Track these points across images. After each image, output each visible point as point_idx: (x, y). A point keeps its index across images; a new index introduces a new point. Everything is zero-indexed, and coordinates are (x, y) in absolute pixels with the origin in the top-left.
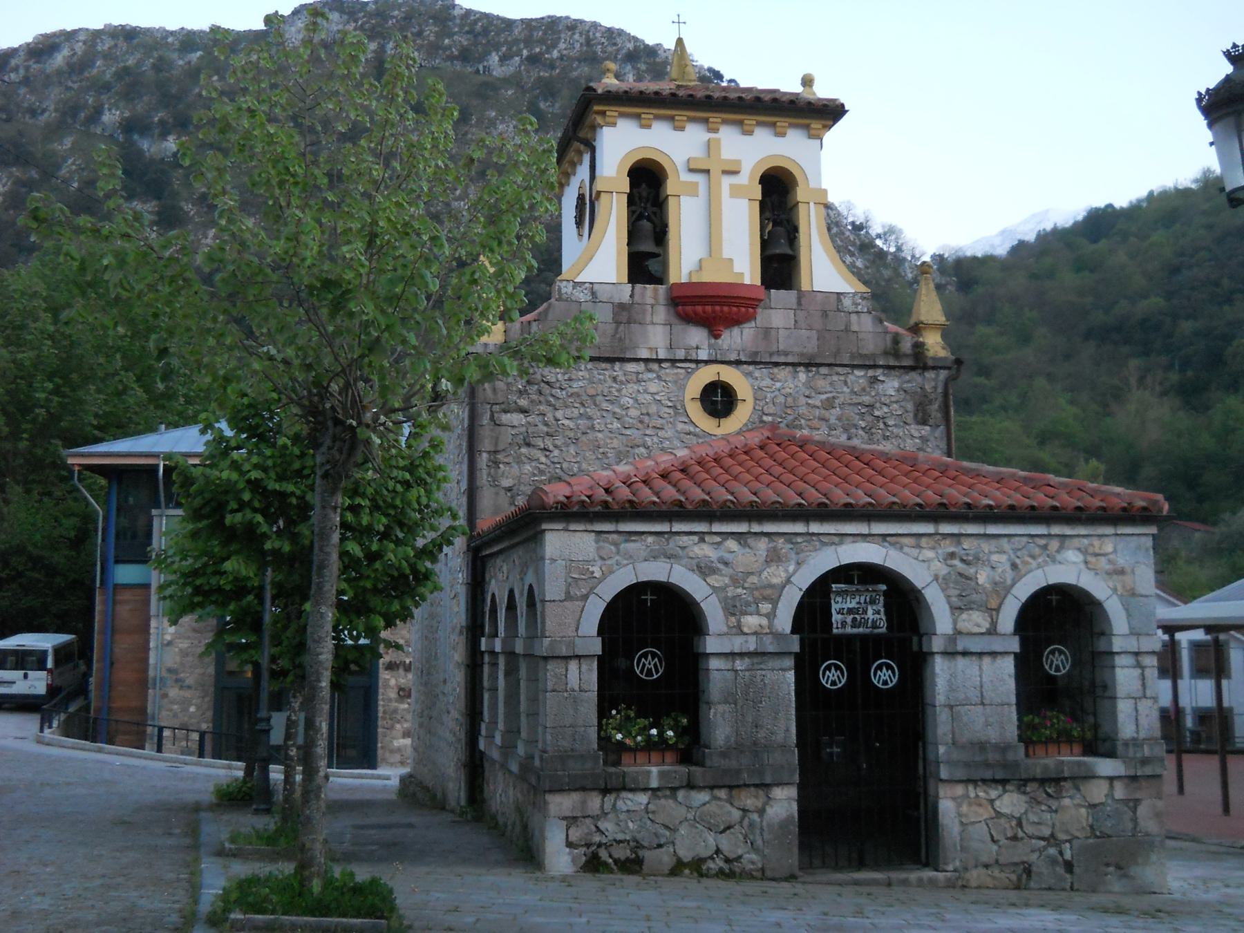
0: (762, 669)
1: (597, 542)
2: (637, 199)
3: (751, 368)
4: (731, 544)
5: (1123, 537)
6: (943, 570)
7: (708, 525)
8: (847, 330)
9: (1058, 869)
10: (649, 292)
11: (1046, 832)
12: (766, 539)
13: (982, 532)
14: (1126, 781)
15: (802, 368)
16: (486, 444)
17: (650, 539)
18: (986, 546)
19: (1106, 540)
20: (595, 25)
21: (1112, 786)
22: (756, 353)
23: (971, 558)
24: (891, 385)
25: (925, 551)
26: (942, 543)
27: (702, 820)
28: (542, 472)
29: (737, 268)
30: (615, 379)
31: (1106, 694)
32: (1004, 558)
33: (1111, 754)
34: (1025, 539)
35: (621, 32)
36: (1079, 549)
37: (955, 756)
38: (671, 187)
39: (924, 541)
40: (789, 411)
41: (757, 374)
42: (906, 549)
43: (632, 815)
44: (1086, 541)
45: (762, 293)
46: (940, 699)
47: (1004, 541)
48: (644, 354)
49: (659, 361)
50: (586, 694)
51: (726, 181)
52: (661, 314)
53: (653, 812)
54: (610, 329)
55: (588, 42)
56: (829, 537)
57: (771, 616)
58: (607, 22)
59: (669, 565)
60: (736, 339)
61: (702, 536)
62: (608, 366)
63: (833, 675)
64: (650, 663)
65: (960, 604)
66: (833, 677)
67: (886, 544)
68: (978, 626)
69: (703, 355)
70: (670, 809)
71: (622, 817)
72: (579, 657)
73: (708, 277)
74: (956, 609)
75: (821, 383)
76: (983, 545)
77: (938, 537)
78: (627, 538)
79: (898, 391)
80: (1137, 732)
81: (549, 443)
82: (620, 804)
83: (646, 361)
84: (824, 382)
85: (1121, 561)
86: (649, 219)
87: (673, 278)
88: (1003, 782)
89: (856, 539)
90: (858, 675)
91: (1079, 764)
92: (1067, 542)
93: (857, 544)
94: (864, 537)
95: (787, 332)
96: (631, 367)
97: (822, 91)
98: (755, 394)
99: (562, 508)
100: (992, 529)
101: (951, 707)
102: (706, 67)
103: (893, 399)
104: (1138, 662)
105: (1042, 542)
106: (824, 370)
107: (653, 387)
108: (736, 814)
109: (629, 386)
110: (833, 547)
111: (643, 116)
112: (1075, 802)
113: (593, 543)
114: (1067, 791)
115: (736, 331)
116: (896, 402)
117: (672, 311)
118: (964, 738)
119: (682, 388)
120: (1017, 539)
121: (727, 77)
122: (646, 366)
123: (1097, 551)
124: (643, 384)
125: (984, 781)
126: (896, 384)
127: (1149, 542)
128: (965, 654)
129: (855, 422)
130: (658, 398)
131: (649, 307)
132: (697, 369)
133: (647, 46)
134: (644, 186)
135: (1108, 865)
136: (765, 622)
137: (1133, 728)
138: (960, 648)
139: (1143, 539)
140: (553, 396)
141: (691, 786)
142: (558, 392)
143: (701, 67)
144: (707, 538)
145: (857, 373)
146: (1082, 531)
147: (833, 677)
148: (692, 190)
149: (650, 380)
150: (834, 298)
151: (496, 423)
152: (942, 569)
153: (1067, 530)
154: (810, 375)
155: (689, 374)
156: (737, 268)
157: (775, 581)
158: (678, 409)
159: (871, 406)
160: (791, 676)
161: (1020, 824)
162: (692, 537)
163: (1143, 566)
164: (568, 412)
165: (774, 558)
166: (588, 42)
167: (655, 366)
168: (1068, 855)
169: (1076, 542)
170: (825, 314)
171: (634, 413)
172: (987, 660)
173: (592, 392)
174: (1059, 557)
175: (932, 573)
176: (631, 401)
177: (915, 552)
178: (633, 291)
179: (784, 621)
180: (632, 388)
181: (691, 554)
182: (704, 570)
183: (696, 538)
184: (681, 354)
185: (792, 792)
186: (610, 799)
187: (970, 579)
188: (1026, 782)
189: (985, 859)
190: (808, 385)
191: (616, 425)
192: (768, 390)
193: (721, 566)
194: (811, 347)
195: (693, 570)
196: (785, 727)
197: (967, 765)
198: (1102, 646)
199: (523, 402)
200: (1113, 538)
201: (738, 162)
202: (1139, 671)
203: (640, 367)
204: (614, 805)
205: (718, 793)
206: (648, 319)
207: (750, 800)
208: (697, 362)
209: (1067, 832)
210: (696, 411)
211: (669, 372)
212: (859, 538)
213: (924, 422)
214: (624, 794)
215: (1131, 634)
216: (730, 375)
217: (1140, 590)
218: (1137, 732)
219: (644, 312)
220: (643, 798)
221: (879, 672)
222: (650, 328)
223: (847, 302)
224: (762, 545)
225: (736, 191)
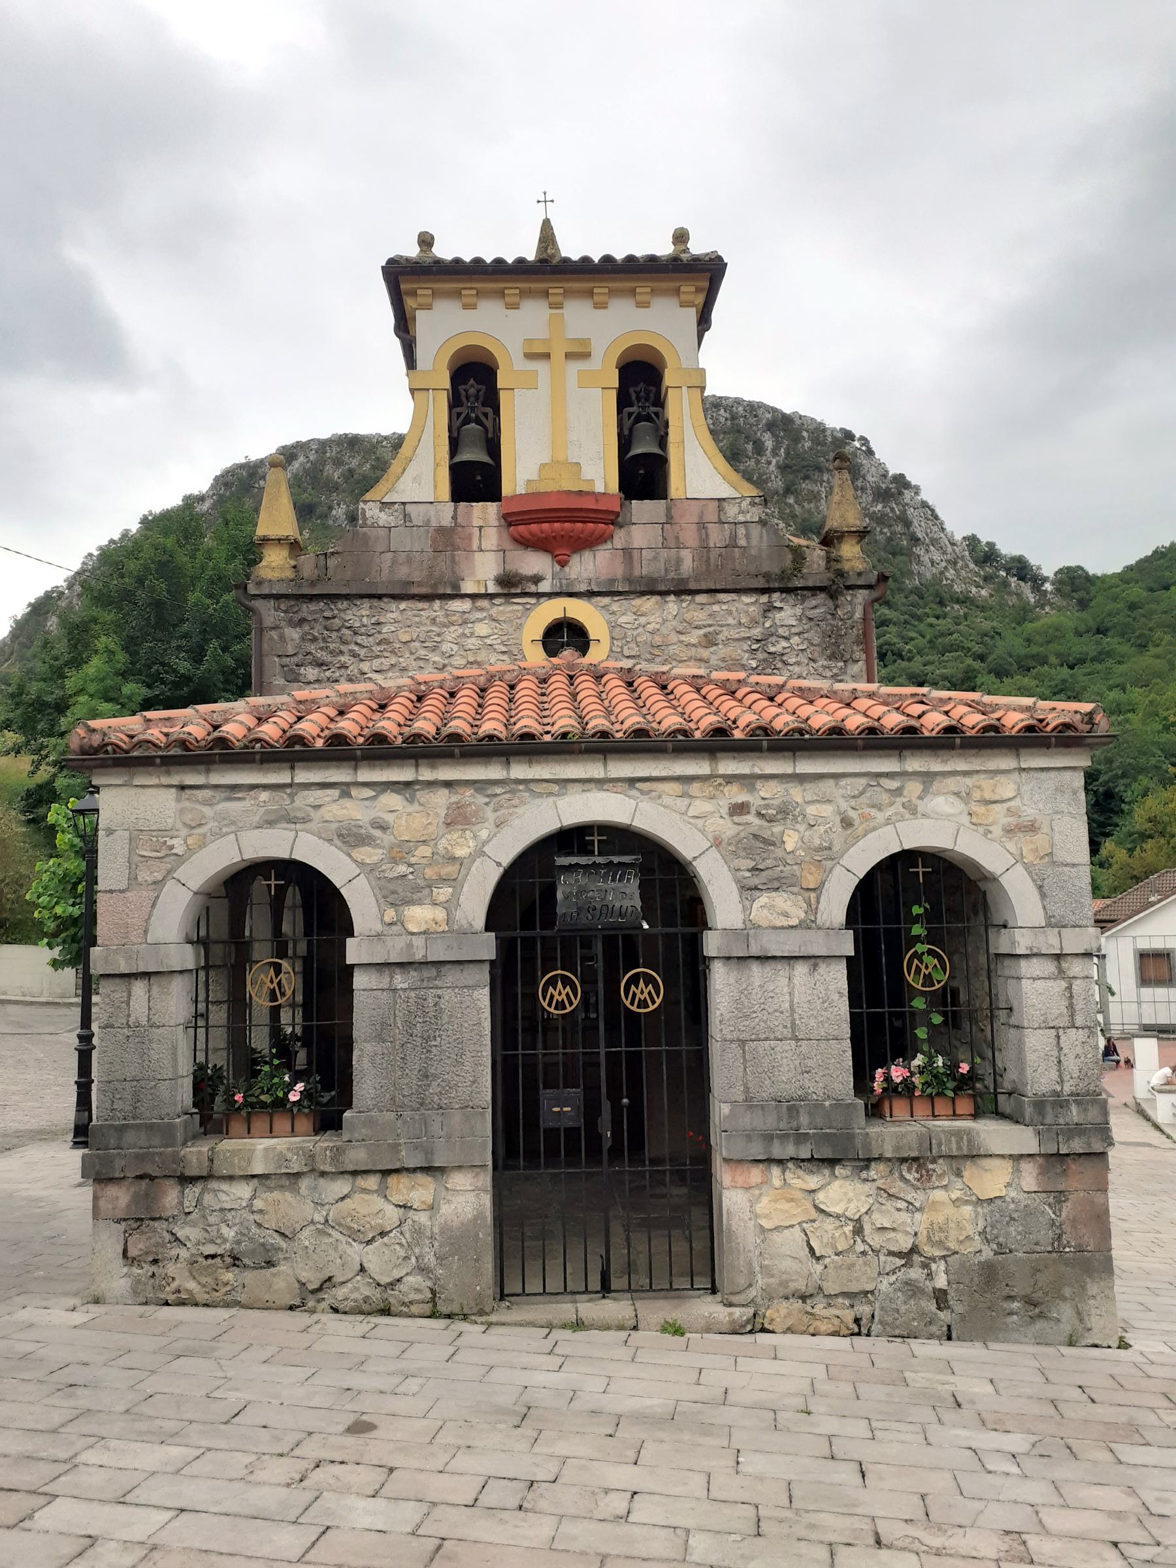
0: (437, 988)
1: (178, 800)
2: (464, 399)
3: (606, 600)
4: (392, 800)
5: (1032, 773)
6: (727, 828)
7: (351, 771)
9: (923, 1303)
10: (485, 513)
11: (905, 1244)
12: (446, 791)
13: (789, 770)
14: (1040, 1160)
15: (672, 598)
17: (264, 796)
18: (797, 793)
19: (1002, 779)
20: (738, 401)
21: (1017, 1171)
22: (613, 581)
23: (772, 812)
24: (788, 613)
25: (697, 802)
26: (726, 789)
27: (340, 1225)
30: (434, 621)
31: (1013, 1021)
32: (827, 810)
33: (1014, 1118)
34: (863, 781)
35: (761, 405)
36: (957, 794)
37: (747, 1120)
39: (695, 788)
40: (656, 652)
41: (615, 607)
42: (666, 800)
43: (229, 1216)
44: (969, 781)
47: (827, 786)
49: (491, 596)
50: (162, 1030)
51: (575, 367)
52: (492, 538)
53: (261, 1211)
55: (734, 417)
56: (545, 785)
57: (449, 906)
58: (748, 397)
59: (293, 834)
61: (345, 789)
62: (425, 605)
63: (560, 993)
65: (756, 881)
67: (634, 792)
68: (786, 915)
69: (545, 587)
71: (212, 1219)
72: (147, 975)
74: (748, 890)
75: (699, 616)
76: (792, 791)
77: (720, 780)
78: (227, 794)
79: (800, 620)
80: (1061, 1082)
82: (208, 1198)
84: (696, 610)
85: (1030, 812)
86: (478, 422)
87: (506, 490)
88: (832, 1162)
89: (587, 786)
91: (958, 1134)
92: (936, 785)
93: (589, 794)
94: (600, 783)
95: (652, 553)
96: (457, 605)
97: (697, 247)
98: (611, 632)
99: (115, 752)
100: (806, 766)
101: (743, 1042)
102: (838, 428)
103: (794, 630)
104: (1061, 971)
105: (894, 784)
107: (482, 629)
108: (392, 1215)
109: (452, 628)
110: (551, 799)
111: (464, 292)
112: (954, 1197)
113: (173, 804)
114: (941, 1176)
115: (587, 555)
116: (798, 634)
117: (505, 534)
118: (766, 1091)
119: (519, 627)
120: (849, 780)
121: (857, 436)
122: (473, 603)
123: (988, 796)
124: (470, 625)
125: (798, 1161)
126: (798, 611)
127: (1079, 780)
128: (764, 959)
129: (744, 662)
130: (488, 641)
131: (476, 531)
132: (538, 604)
133: (784, 415)
134: (472, 381)
135: (1010, 1298)
136: (440, 914)
137: (1054, 1075)
138: (755, 951)
139: (1067, 775)
140: (356, 644)
143: (834, 430)
144: (354, 792)
145: (747, 599)
146: (961, 765)
149: (481, 620)
152: (727, 828)
153: (936, 766)
154: (684, 605)
157: (460, 852)
160: (483, 997)
161: (858, 1231)
162: (329, 791)
163: (1067, 819)
164: (376, 664)
165: (457, 819)
166: (734, 417)
167: (485, 603)
168: (941, 1282)
169: (951, 783)
170: (702, 526)
172: (801, 969)
174: (922, 806)
175: (710, 836)
176: (455, 647)
177: (682, 803)
178: (455, 510)
180: (457, 630)
181: (328, 817)
183: (335, 793)
186: (193, 1192)
187: (774, 844)
188: (867, 1162)
189: (800, 1285)
192: (629, 626)
193: (377, 833)
195: (330, 841)
197: (768, 1138)
198: (1002, 943)
200: (1015, 776)
201: (586, 342)
202: (1064, 984)
203: (466, 605)
204: (199, 1202)
205: (361, 1182)
206: (475, 547)
207: (420, 1191)
209: (940, 1244)
211: (500, 609)
212: (593, 785)
214: (214, 1185)
215: (1049, 925)
216: (579, 610)
217: (1061, 855)
218: (1061, 1082)
219: (470, 538)
220: (243, 1191)
221: (551, 989)
222: (478, 555)
224: (441, 798)
225: (586, 381)
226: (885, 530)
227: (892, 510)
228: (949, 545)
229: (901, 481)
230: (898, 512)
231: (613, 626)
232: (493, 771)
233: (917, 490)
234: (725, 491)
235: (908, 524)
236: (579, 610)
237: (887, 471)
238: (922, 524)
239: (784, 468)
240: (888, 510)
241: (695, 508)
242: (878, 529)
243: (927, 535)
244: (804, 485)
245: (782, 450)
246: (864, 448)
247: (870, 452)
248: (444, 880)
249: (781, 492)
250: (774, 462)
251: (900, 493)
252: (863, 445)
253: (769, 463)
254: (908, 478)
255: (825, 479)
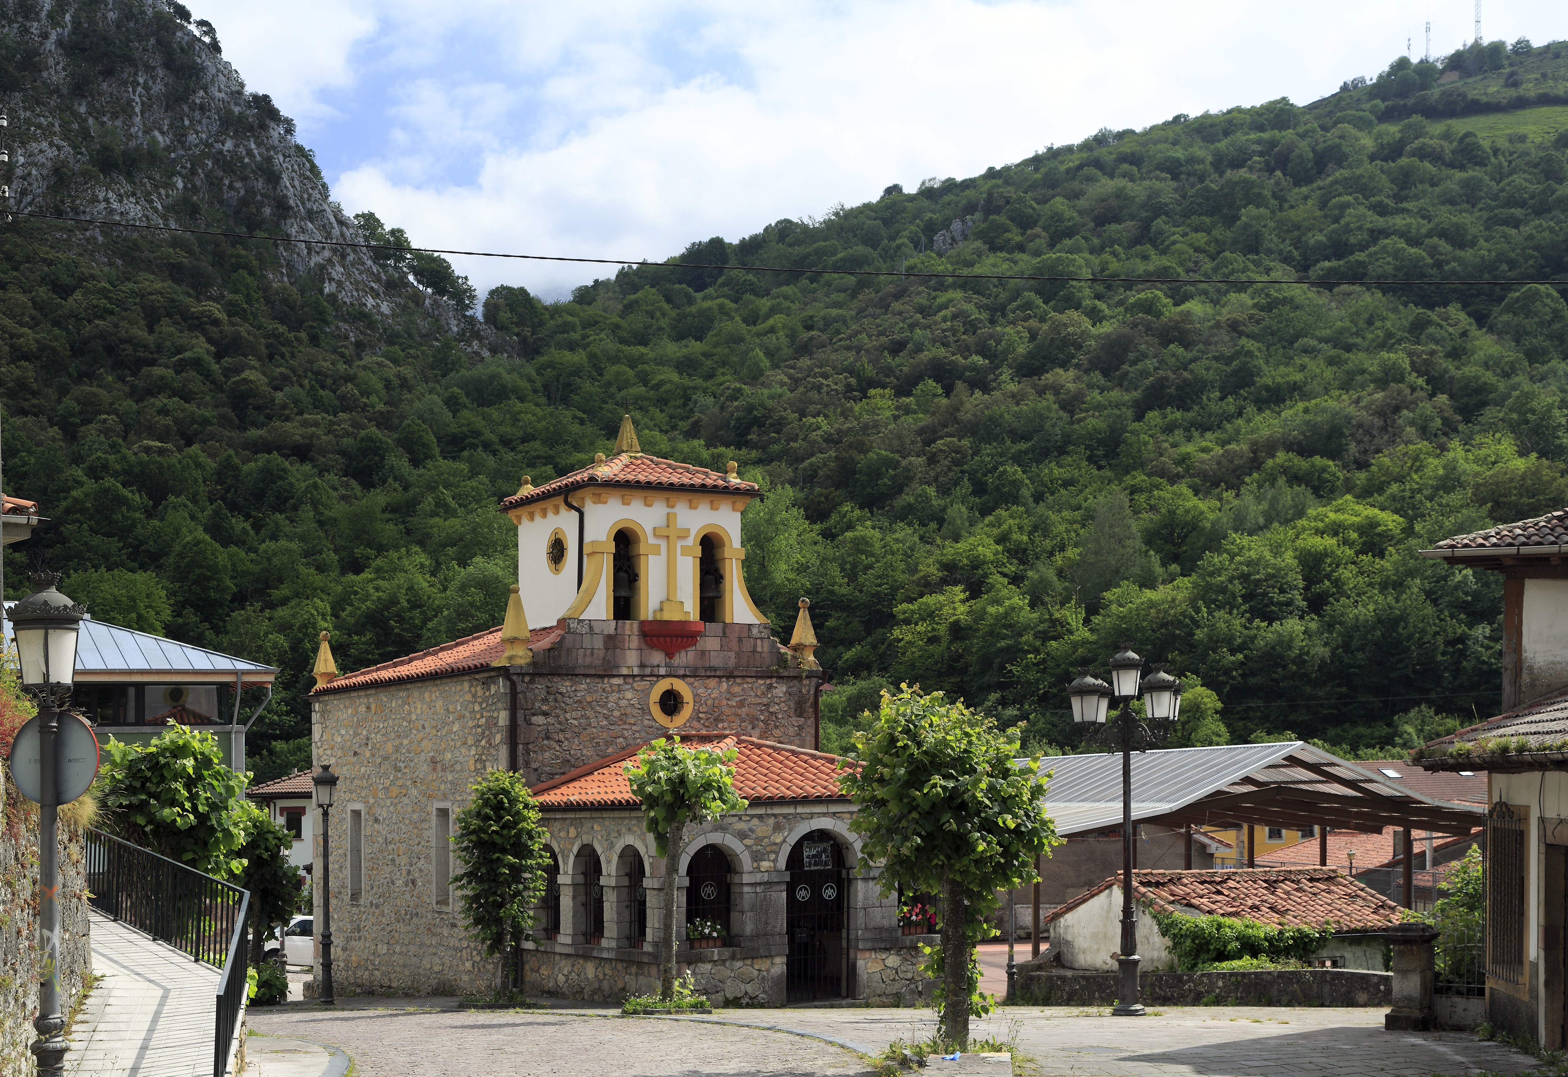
4: (755, 821)
8: (754, 651)
11: (910, 976)
16: (521, 739)
24: (780, 690)
28: (557, 757)
29: (687, 608)
37: (868, 935)
38: (642, 549)
45: (701, 626)
46: (860, 904)
48: (625, 671)
49: (634, 676)
52: (635, 642)
54: (602, 654)
57: (775, 861)
60: (685, 658)
64: (709, 890)
66: (803, 895)
69: (662, 671)
70: (724, 972)
73: (667, 616)
75: (736, 689)
81: (561, 736)
83: (625, 676)
88: (886, 949)
90: (816, 893)
94: (825, 814)
96: (616, 681)
106: (738, 680)
121: (196, 16)
141: (733, 958)
142: (569, 701)
147: (803, 895)
148: (657, 551)
150: (746, 628)
151: (529, 723)
155: (652, 685)
156: (687, 608)
158: (645, 710)
159: (767, 705)
160: (784, 894)
165: (777, 828)
170: (740, 640)
171: (616, 713)
173: (589, 699)
179: (782, 864)
182: (742, 835)
184: (648, 671)
185: (784, 959)
190: (728, 691)
191: (605, 723)
194: (732, 662)
196: (781, 923)
199: (544, 708)
203: (620, 681)
208: (658, 676)
210: (656, 711)
211: (639, 685)
213: (800, 715)
216: (680, 686)
220: (708, 966)
223: (755, 631)
224: (772, 821)
225: (685, 551)
226: (238, 185)
227: (250, 153)
228: (335, 225)
229: (263, 103)
230: (258, 158)
231: (696, 695)
232: (790, 810)
233: (289, 126)
234: (756, 621)
235: (273, 178)
236: (680, 686)
237: (242, 85)
238: (296, 183)
239: (70, 48)
240: (241, 149)
241: (737, 628)
242: (227, 182)
243: (303, 203)
244: (105, 86)
245: (68, 17)
246: (207, 39)
247: (215, 47)
248: (772, 852)
249: (65, 91)
250: (53, 37)
251: (263, 127)
252: (206, 33)
253: (45, 36)
254: (277, 103)
255: (141, 80)
